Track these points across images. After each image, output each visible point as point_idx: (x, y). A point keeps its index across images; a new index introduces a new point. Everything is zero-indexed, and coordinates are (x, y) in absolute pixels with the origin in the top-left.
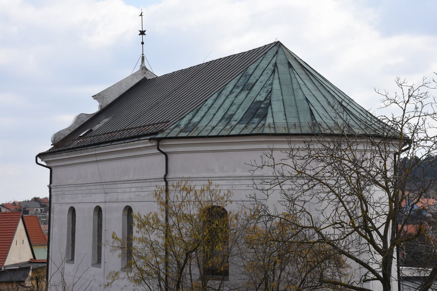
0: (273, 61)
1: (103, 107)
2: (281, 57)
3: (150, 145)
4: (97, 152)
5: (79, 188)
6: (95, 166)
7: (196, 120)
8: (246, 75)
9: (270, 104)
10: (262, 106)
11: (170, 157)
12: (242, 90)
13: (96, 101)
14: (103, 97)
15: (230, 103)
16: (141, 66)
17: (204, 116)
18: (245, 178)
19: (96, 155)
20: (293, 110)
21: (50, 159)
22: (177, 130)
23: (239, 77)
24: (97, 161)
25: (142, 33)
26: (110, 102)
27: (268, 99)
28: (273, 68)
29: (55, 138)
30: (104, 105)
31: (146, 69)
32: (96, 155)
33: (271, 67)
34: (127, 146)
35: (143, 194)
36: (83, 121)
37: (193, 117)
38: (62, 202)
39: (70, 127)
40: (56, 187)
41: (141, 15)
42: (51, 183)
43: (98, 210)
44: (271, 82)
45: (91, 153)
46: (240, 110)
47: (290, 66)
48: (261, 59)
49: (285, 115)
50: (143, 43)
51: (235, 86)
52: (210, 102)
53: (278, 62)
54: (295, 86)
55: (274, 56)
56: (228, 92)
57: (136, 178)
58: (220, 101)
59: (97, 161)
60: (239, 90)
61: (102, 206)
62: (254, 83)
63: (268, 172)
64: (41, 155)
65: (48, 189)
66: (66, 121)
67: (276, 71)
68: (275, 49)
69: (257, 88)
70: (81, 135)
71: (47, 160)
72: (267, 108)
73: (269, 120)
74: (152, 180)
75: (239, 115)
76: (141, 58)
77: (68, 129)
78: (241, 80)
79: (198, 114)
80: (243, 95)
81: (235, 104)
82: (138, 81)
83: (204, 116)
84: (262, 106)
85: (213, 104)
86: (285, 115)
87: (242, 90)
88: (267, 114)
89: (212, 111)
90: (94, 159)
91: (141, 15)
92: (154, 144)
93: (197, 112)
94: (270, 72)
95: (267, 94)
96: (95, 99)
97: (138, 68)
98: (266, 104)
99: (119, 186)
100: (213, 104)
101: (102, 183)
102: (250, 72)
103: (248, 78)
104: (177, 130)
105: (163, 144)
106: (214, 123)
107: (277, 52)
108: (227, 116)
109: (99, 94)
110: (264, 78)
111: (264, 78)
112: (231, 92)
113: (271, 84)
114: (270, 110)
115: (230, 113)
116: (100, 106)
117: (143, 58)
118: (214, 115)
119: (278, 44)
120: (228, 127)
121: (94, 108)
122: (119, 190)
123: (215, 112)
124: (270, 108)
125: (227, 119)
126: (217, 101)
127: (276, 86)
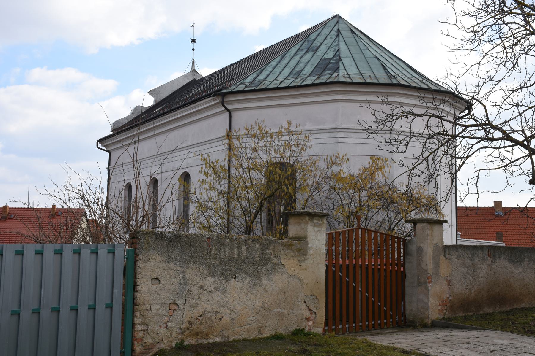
0: (336, 28)
1: (157, 102)
2: (341, 26)
3: (213, 103)
6: (153, 140)
7: (261, 77)
8: (308, 41)
9: (340, 59)
10: (332, 61)
11: (234, 114)
12: (307, 52)
13: (151, 96)
14: (158, 93)
15: (296, 62)
16: (191, 69)
17: (270, 74)
18: (315, 132)
20: (365, 65)
21: (109, 143)
22: (244, 86)
23: (301, 43)
25: (193, 41)
26: (164, 97)
27: (337, 56)
28: (336, 34)
29: (114, 125)
30: (159, 100)
31: (196, 72)
32: (154, 128)
33: (334, 33)
34: (187, 111)
36: (139, 112)
37: (258, 76)
39: (128, 117)
41: (193, 26)
42: (109, 165)
44: (337, 43)
45: (148, 128)
46: (308, 67)
48: (322, 28)
49: (358, 68)
50: (193, 50)
51: (299, 49)
52: (274, 63)
53: (340, 29)
54: (362, 47)
55: (335, 25)
56: (292, 55)
57: (195, 142)
58: (285, 61)
59: (155, 135)
60: (304, 52)
61: (158, 177)
63: (341, 124)
64: (100, 141)
65: (107, 171)
66: (123, 112)
67: (340, 35)
68: (335, 20)
69: (322, 49)
71: (107, 144)
72: (338, 63)
73: (342, 71)
74: (213, 141)
75: (308, 70)
77: (126, 118)
78: (304, 45)
79: (262, 73)
80: (308, 56)
81: (301, 63)
83: (270, 74)
84: (332, 61)
85: (277, 65)
86: (358, 68)
87: (307, 52)
88: (339, 67)
89: (278, 70)
91: (193, 26)
92: (218, 101)
93: (262, 71)
94: (334, 37)
95: (335, 53)
96: (150, 94)
97: (189, 70)
98: (336, 60)
99: (176, 154)
100: (277, 65)
102: (313, 38)
103: (310, 43)
104: (244, 86)
105: (227, 100)
106: (282, 77)
107: (338, 22)
108: (294, 72)
109: (154, 90)
110: (329, 41)
111: (329, 41)
112: (295, 54)
113: (338, 45)
114: (341, 64)
115: (297, 69)
116: (155, 100)
117: (193, 62)
118: (281, 72)
119: (337, 18)
120: (299, 80)
121: (149, 102)
122: (176, 159)
123: (281, 70)
124: (340, 63)
125: (295, 74)
126: (281, 62)
127: (342, 46)
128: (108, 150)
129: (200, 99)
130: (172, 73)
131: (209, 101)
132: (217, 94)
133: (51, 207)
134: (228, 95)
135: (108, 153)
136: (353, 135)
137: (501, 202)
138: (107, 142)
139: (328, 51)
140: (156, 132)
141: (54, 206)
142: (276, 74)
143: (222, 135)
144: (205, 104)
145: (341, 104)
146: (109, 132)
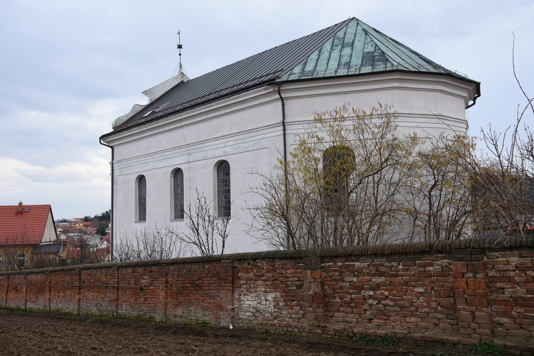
4: (181, 118)
5: (149, 157)
14: (152, 93)
16: (179, 72)
19: (181, 120)
24: (182, 127)
29: (116, 123)
31: (183, 74)
32: (181, 120)
35: (245, 145)
36: (137, 110)
38: (127, 173)
40: (120, 161)
43: (177, 173)
47: (366, 33)
50: (180, 55)
59: (182, 127)
62: (351, 41)
64: (103, 137)
70: (146, 115)
71: (109, 140)
76: (179, 66)
77: (126, 116)
82: (177, 83)
90: (179, 125)
91: (179, 33)
96: (145, 94)
97: (177, 74)
99: (207, 144)
101: (187, 145)
116: (151, 100)
117: (181, 66)
121: (145, 101)
122: (208, 148)
128: (110, 145)
129: (247, 89)
130: (161, 76)
131: (260, 91)
132: (271, 82)
133: (18, 204)
134: (284, 85)
135: (110, 149)
136: (408, 119)
137: (48, 208)
138: (112, 138)
139: (366, 46)
140: (183, 124)
141: (20, 204)
142: (326, 63)
143: (280, 122)
144: (252, 94)
145: (395, 91)
146: (111, 130)
